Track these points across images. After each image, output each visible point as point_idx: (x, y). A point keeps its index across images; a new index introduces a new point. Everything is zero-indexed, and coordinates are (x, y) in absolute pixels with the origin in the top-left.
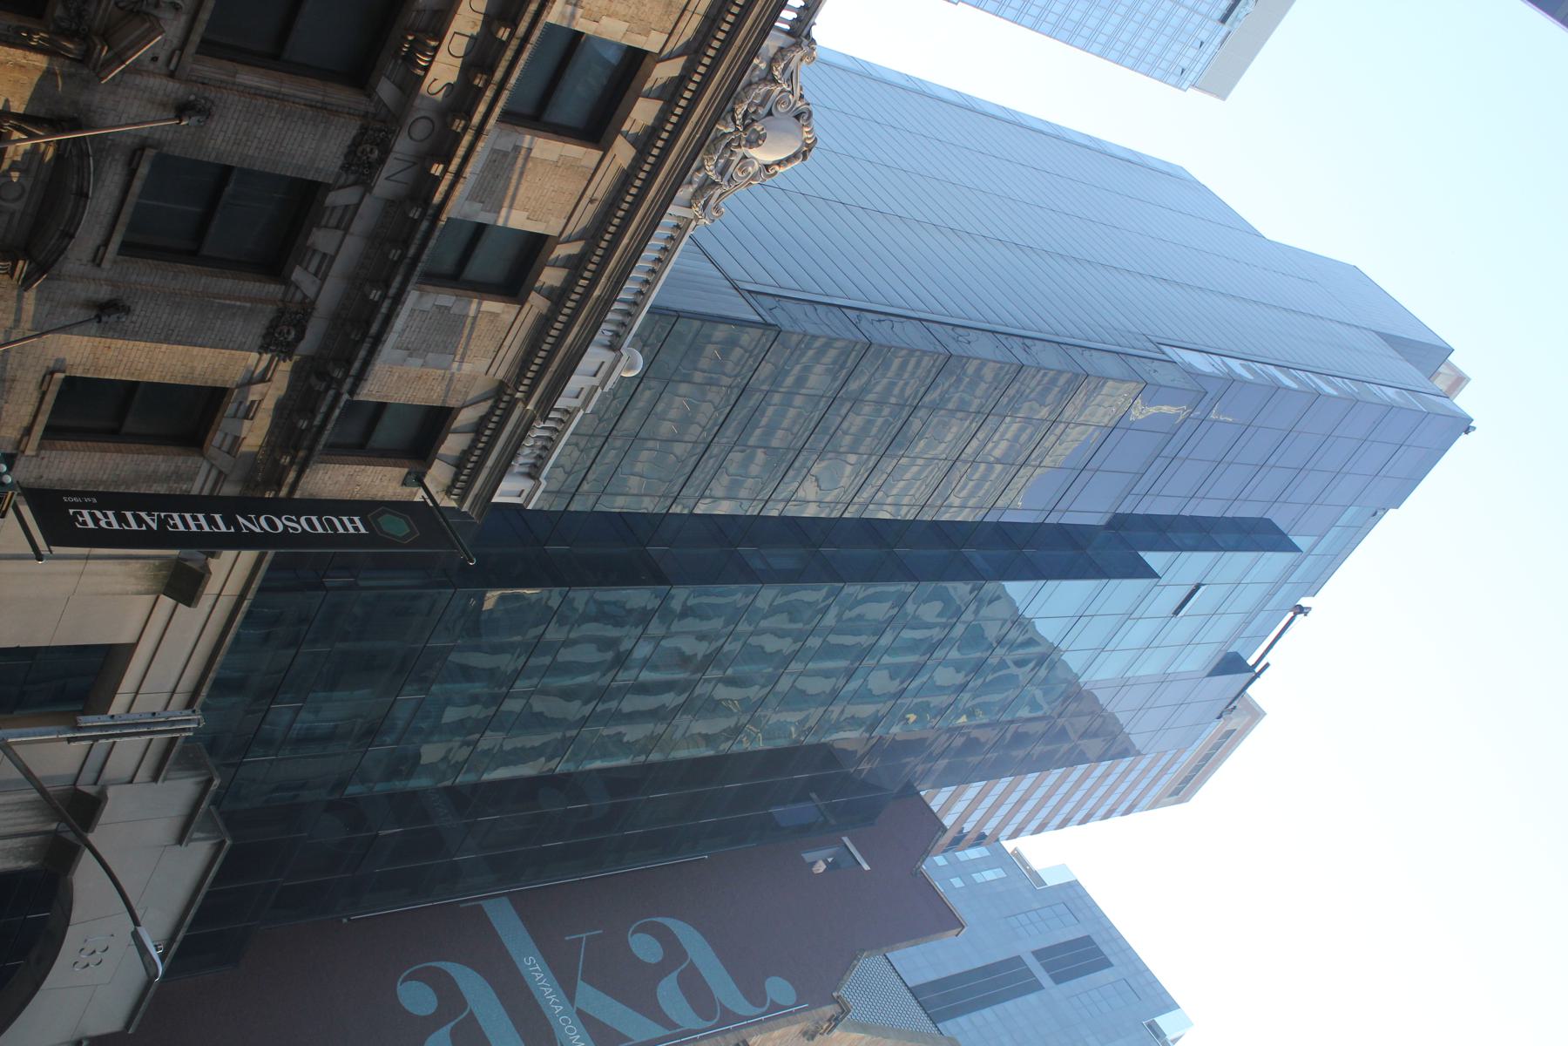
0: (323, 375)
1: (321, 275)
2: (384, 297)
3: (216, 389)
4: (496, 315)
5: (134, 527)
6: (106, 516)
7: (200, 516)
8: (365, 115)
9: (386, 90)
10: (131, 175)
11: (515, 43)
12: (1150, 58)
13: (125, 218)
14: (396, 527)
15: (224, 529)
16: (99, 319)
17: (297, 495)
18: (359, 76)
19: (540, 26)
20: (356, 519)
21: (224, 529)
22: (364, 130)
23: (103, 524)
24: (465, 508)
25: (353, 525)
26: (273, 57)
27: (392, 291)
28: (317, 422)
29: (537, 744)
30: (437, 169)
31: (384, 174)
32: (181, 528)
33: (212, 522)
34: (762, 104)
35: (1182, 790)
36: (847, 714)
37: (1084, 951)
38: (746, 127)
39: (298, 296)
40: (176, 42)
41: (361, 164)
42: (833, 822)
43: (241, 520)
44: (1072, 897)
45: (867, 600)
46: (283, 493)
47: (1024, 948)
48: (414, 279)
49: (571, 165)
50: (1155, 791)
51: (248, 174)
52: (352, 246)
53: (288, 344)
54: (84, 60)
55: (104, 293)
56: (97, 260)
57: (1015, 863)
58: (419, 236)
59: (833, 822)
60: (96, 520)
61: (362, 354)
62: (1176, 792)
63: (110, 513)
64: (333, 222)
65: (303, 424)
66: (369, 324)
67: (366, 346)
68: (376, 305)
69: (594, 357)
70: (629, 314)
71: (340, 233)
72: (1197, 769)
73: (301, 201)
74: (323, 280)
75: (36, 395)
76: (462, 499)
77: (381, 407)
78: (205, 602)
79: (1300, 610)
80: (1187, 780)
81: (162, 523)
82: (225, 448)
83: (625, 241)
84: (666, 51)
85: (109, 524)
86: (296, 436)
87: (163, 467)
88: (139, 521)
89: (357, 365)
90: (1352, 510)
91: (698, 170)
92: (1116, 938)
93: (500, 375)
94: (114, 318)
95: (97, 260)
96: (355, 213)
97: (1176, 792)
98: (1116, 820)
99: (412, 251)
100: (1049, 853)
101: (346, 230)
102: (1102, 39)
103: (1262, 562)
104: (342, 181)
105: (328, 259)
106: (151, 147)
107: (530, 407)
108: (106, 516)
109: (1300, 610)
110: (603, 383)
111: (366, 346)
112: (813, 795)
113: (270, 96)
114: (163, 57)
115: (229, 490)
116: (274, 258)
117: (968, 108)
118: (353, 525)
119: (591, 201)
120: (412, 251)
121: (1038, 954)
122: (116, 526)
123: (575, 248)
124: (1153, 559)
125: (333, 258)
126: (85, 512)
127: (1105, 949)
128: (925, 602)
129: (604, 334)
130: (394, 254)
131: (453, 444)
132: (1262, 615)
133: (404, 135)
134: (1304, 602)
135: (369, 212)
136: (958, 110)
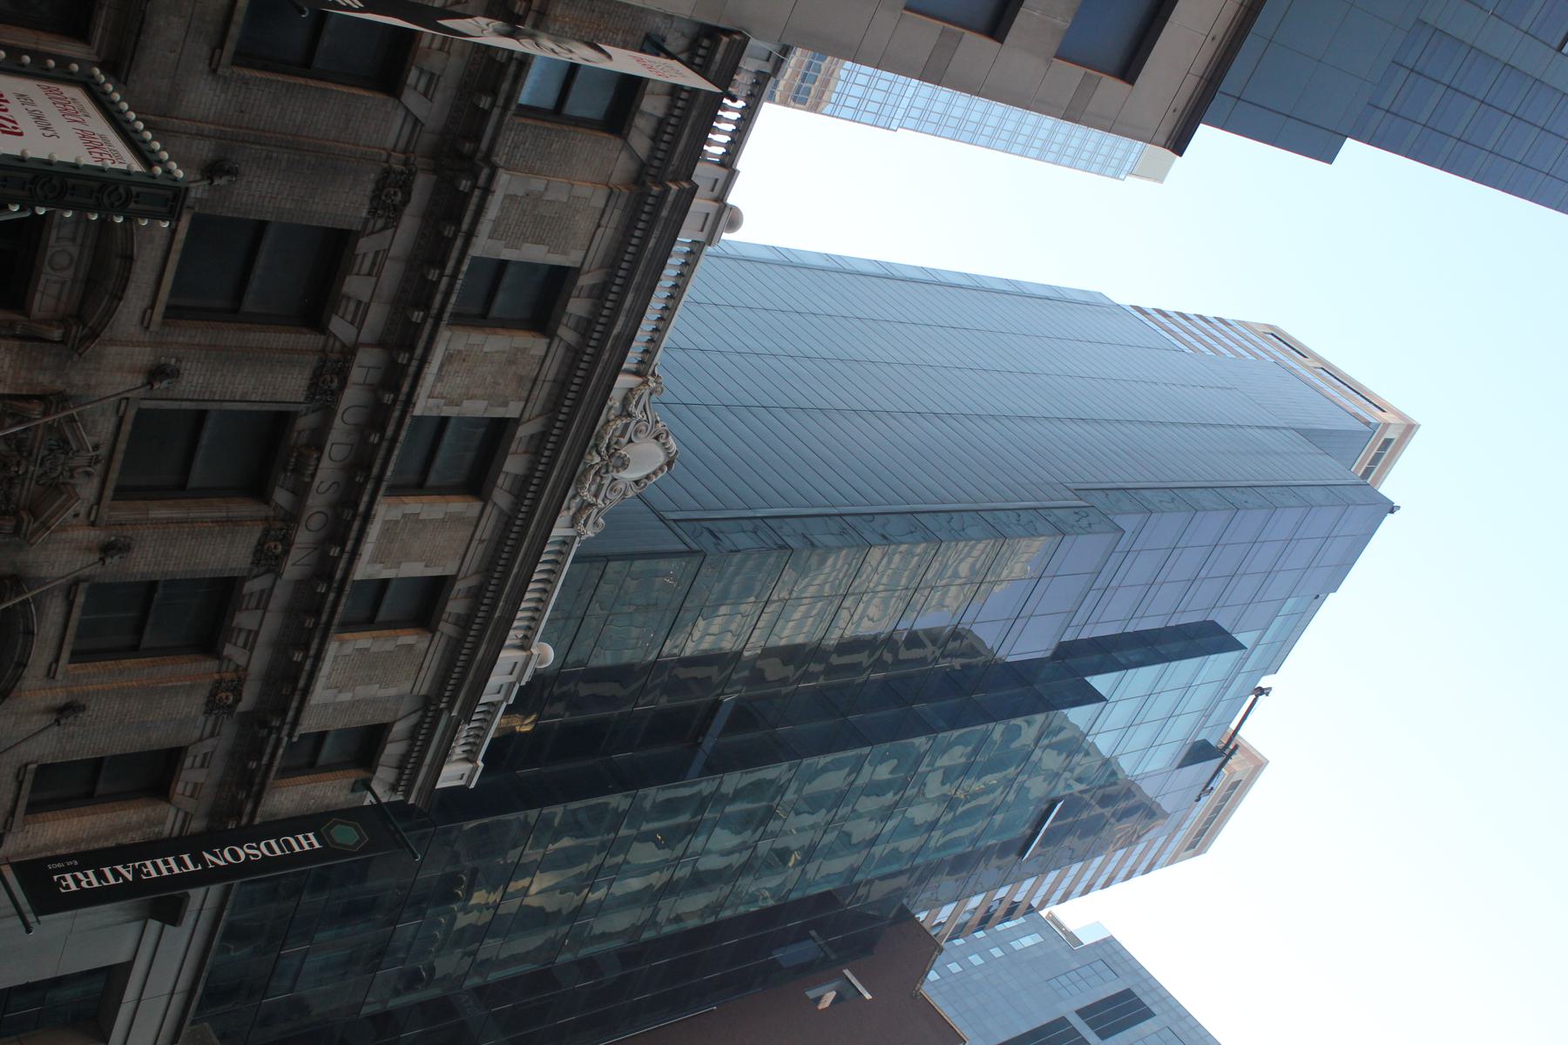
0: (264, 724)
1: (249, 646)
2: (305, 657)
3: (172, 750)
4: (411, 646)
5: (112, 881)
6: (87, 876)
7: (171, 859)
8: (267, 519)
9: (282, 497)
10: (70, 604)
11: (385, 444)
12: (1085, 155)
13: (71, 632)
14: (346, 835)
15: (192, 868)
16: (58, 722)
17: (257, 821)
18: (257, 489)
19: (408, 420)
20: (310, 835)
21: (192, 868)
22: (266, 532)
23: (84, 884)
24: (411, 801)
25: (307, 842)
26: (178, 489)
27: (312, 652)
28: (265, 760)
29: (532, 947)
30: (433, 275)
31: (290, 562)
32: (154, 874)
33: (181, 863)
34: (622, 435)
35: (1198, 843)
36: (823, 872)
37: (1128, 1003)
38: (611, 456)
39: (232, 667)
40: (92, 499)
41: (268, 559)
42: (833, 957)
43: (207, 856)
44: (1109, 952)
45: (825, 770)
46: (244, 821)
47: (1068, 1008)
48: (382, 492)
49: (456, 519)
50: (1173, 846)
51: (172, 583)
52: (272, 623)
53: (277, 557)
54: (17, 531)
55: (59, 697)
56: (50, 674)
57: (1053, 928)
58: (328, 605)
59: (833, 957)
60: (77, 881)
61: (294, 704)
62: (1193, 846)
63: (90, 873)
64: (253, 603)
65: (254, 765)
66: (296, 680)
67: (297, 698)
68: (301, 665)
69: (508, 657)
70: (477, 736)
71: (260, 612)
72: (1210, 821)
73: (222, 594)
74: (251, 650)
75: (13, 787)
76: (407, 793)
77: (321, 736)
78: (189, 919)
79: (1261, 691)
80: (1201, 833)
81: (137, 872)
82: (188, 793)
83: (515, 570)
84: (526, 416)
85: (89, 883)
86: (247, 775)
87: (135, 818)
88: (117, 874)
89: (291, 714)
90: (1291, 602)
91: (574, 497)
92: (1156, 988)
93: (424, 691)
94: (71, 719)
95: (50, 674)
96: (270, 596)
97: (1193, 846)
98: (1137, 880)
99: (324, 618)
100: (1087, 914)
101: (265, 609)
102: (1038, 143)
103: (1209, 664)
104: (255, 572)
105: (253, 635)
106: (85, 580)
107: (454, 714)
108: (87, 876)
109: (1261, 691)
110: (520, 679)
111: (297, 698)
112: (813, 933)
113: (179, 522)
114: (83, 512)
115: (197, 825)
116: (208, 642)
117: (887, 276)
118: (307, 842)
119: (481, 541)
120: (324, 618)
121: (1081, 1013)
122: (96, 884)
123: (473, 581)
124: (1099, 682)
125: (257, 633)
126: (68, 876)
127: (1146, 1000)
128: (881, 762)
129: (514, 636)
130: (309, 623)
131: (393, 750)
132: (1222, 705)
133: (302, 528)
134: (1264, 683)
135: (281, 596)
136: (877, 281)
